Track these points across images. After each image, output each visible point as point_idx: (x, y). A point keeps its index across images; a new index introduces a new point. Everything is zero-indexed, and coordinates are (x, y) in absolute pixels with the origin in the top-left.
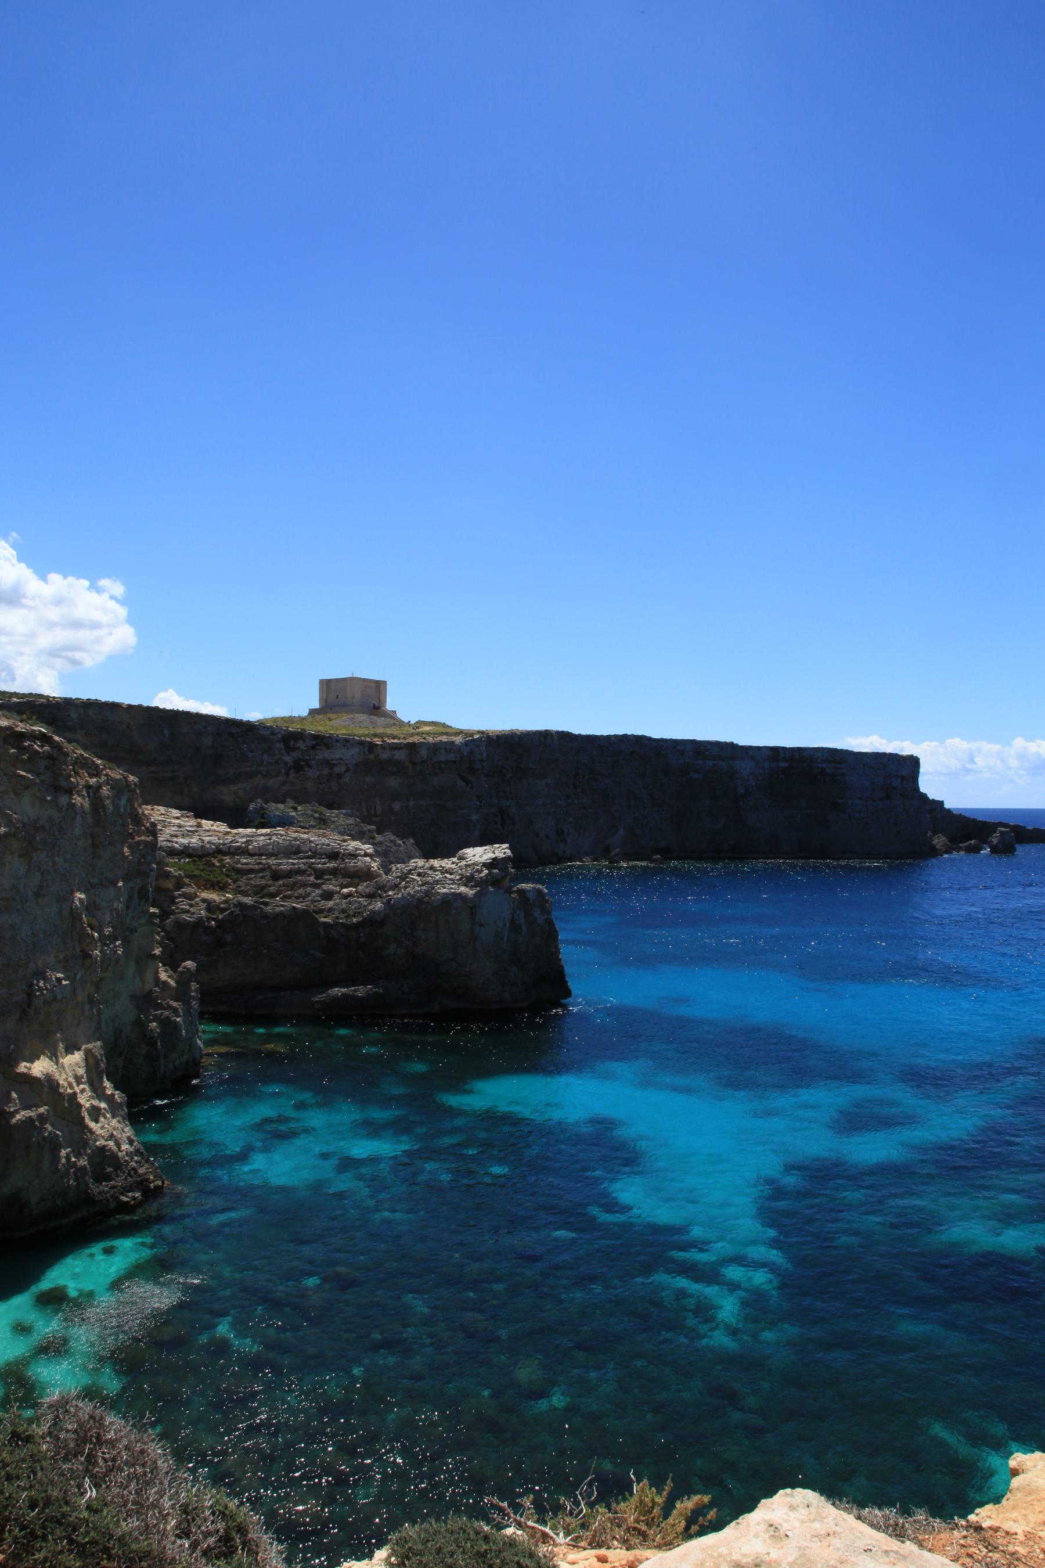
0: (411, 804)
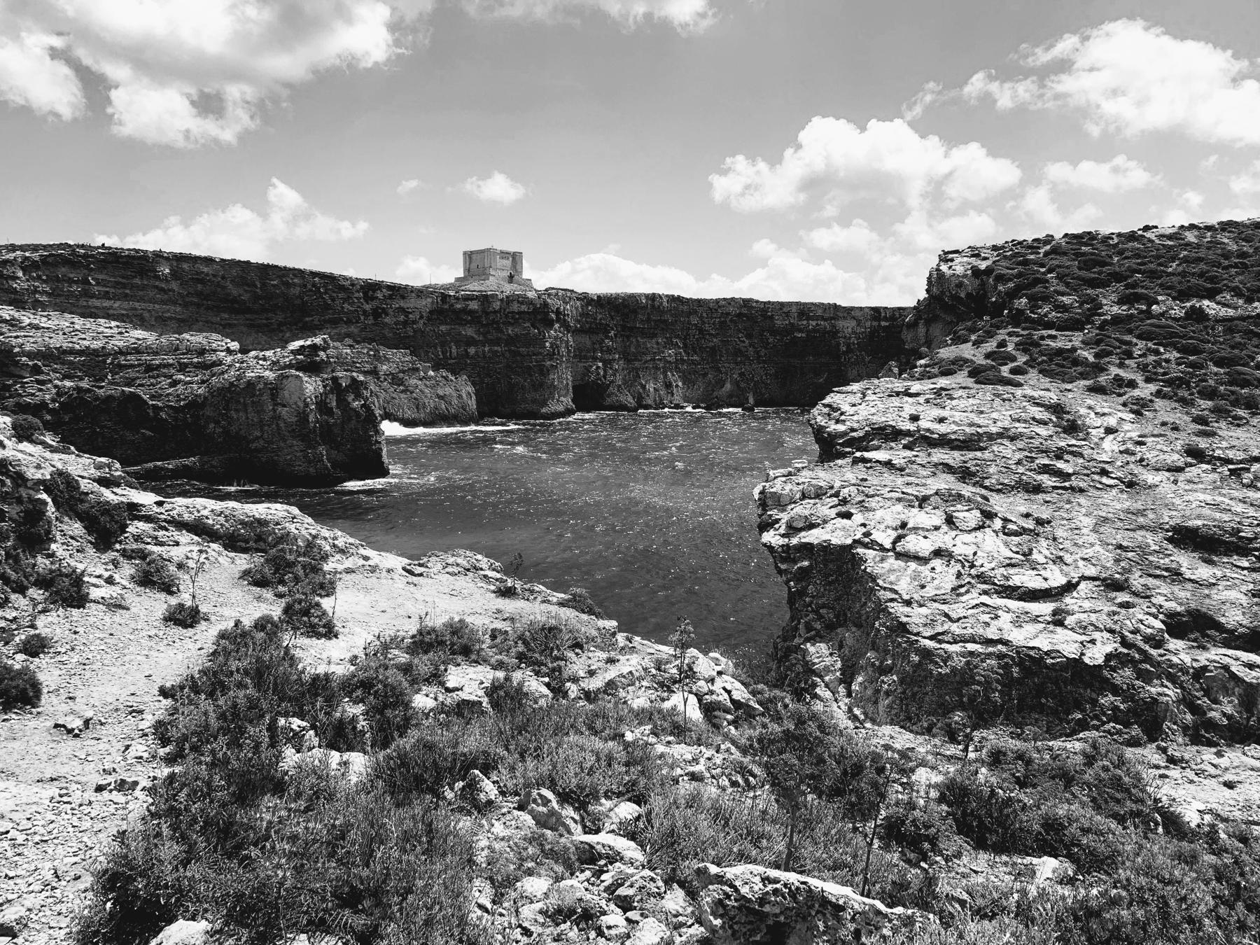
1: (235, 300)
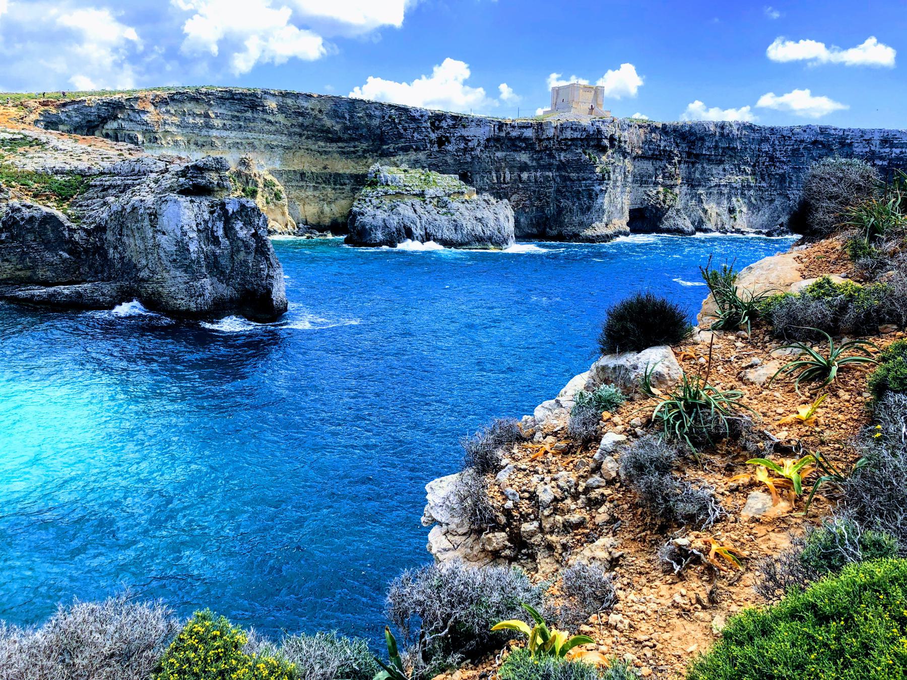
0: (538, 174)
1: (328, 131)
